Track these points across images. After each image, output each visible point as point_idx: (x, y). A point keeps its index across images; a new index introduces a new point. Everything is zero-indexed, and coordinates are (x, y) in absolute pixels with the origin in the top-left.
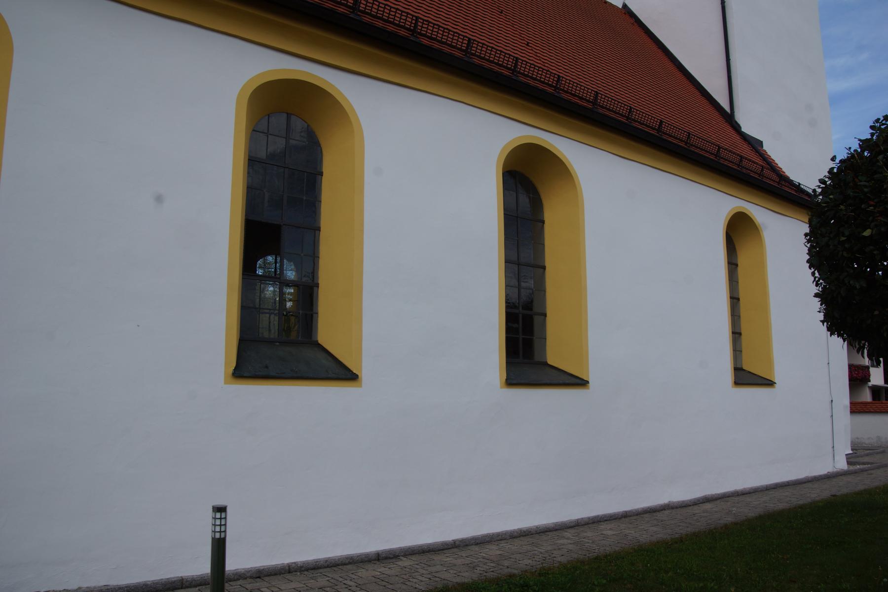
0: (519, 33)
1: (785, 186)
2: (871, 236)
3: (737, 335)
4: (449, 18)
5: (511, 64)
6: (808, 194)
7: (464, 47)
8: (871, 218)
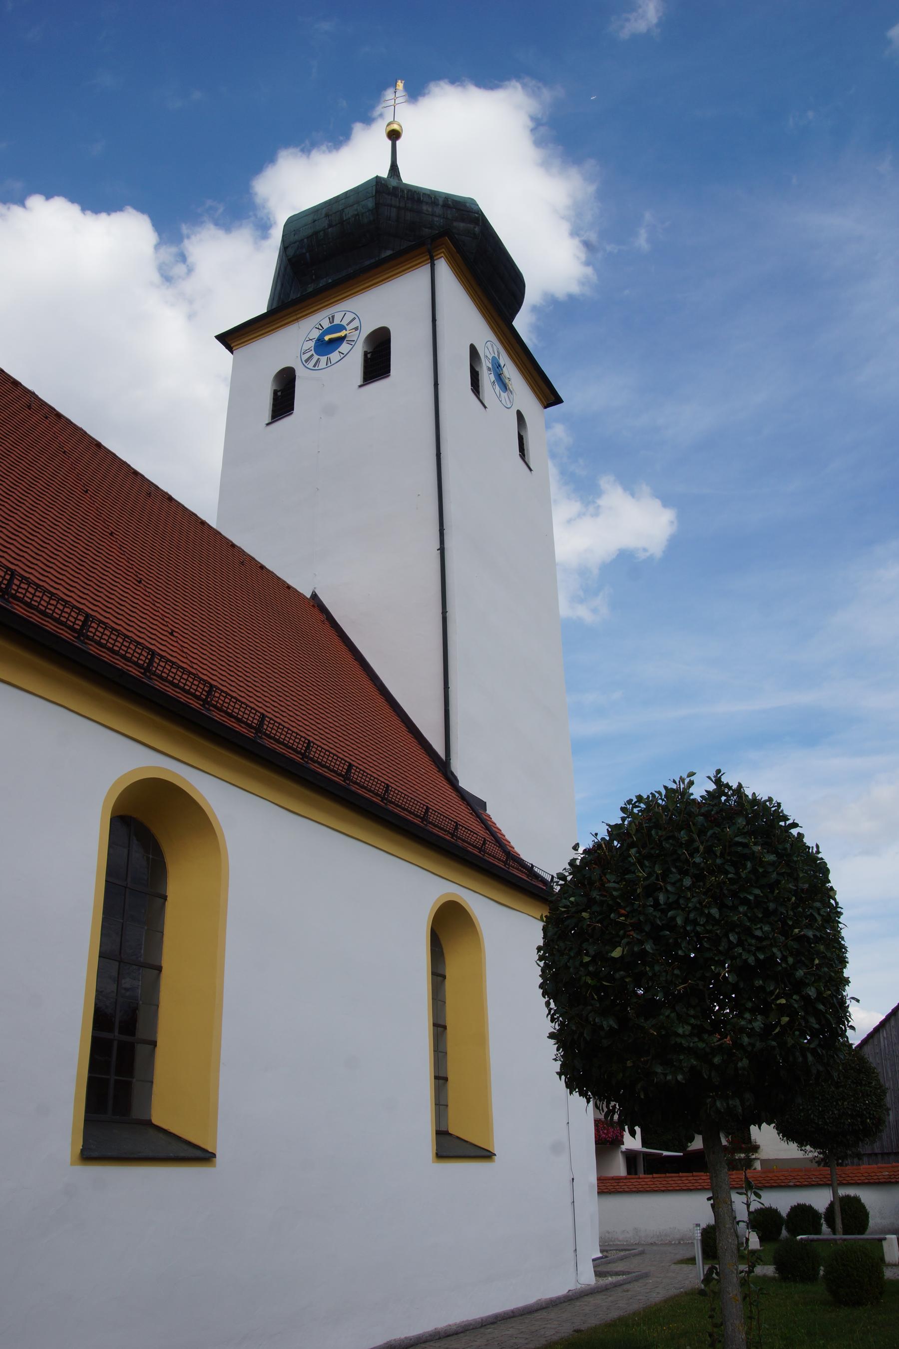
0: (162, 614)
1: (513, 867)
2: (622, 957)
3: (441, 1081)
4: (62, 580)
5: (144, 659)
6: (543, 881)
7: (78, 625)
8: (621, 932)
